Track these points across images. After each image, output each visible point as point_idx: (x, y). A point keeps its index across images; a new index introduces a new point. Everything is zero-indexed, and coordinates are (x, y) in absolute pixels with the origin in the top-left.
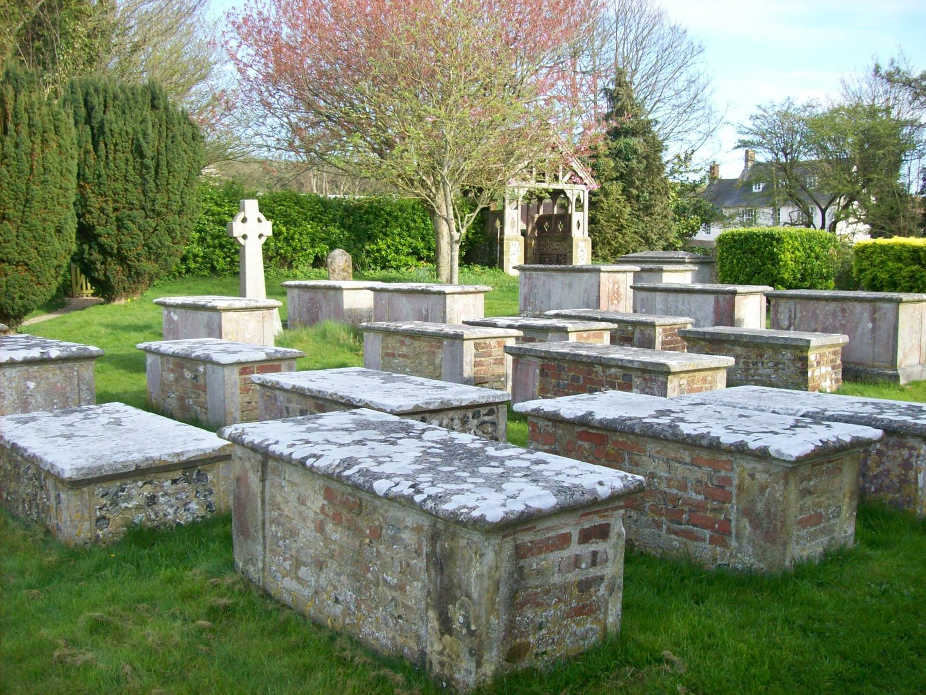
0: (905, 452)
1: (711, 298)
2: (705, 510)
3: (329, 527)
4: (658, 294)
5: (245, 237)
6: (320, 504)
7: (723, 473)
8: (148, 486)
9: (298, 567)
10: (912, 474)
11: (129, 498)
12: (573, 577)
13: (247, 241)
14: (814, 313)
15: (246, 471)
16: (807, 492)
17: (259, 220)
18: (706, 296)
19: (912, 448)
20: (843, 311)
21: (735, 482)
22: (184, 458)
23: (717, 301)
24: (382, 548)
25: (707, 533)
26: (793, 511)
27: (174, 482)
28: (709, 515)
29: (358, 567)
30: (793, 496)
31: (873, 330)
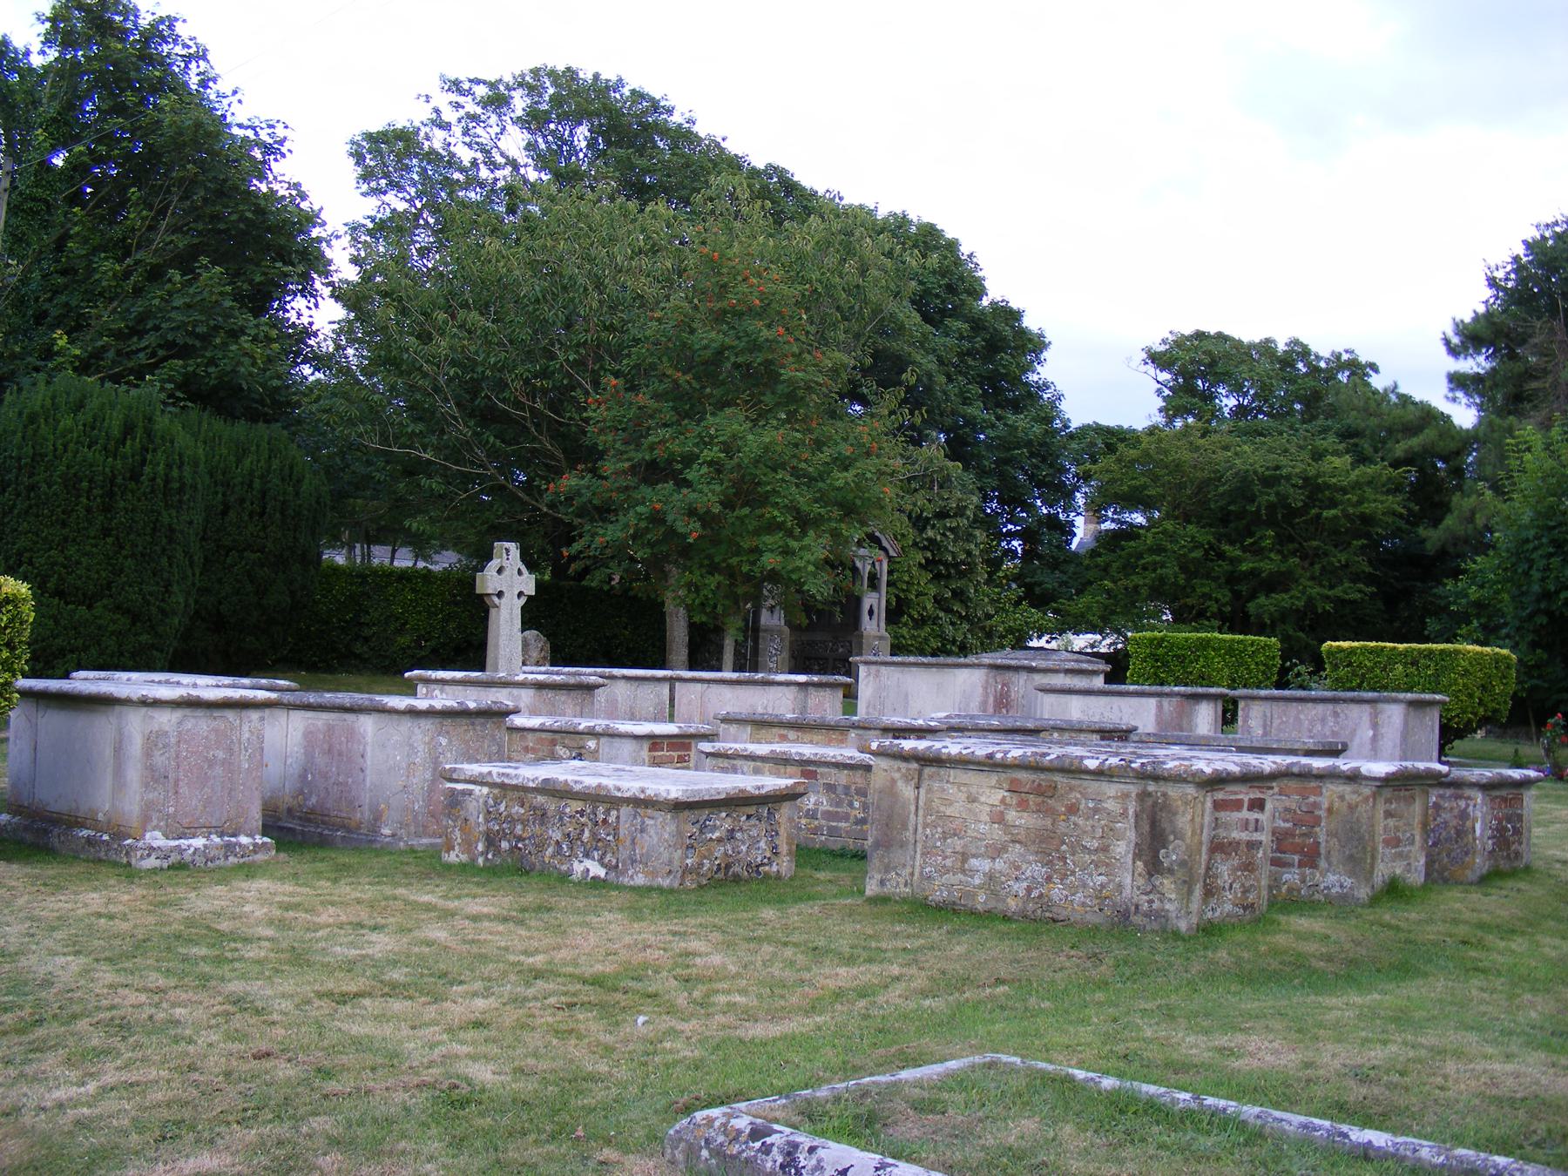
0: (1462, 804)
1: (1153, 702)
2: (1293, 836)
3: (1012, 815)
4: (1074, 697)
5: (500, 594)
6: (1000, 797)
7: (1312, 799)
8: (729, 820)
9: (964, 861)
10: (1469, 824)
11: (715, 828)
12: (1244, 836)
13: (503, 600)
14: (1297, 718)
15: (894, 781)
16: (1388, 814)
17: (520, 572)
18: (1144, 700)
19: (1469, 798)
20: (1336, 715)
21: (1325, 805)
22: (763, 792)
23: (1160, 707)
24: (1081, 822)
25: (1296, 858)
26: (1380, 829)
27: (749, 817)
28: (1297, 840)
29: (1047, 846)
30: (1380, 814)
31: (1374, 739)
